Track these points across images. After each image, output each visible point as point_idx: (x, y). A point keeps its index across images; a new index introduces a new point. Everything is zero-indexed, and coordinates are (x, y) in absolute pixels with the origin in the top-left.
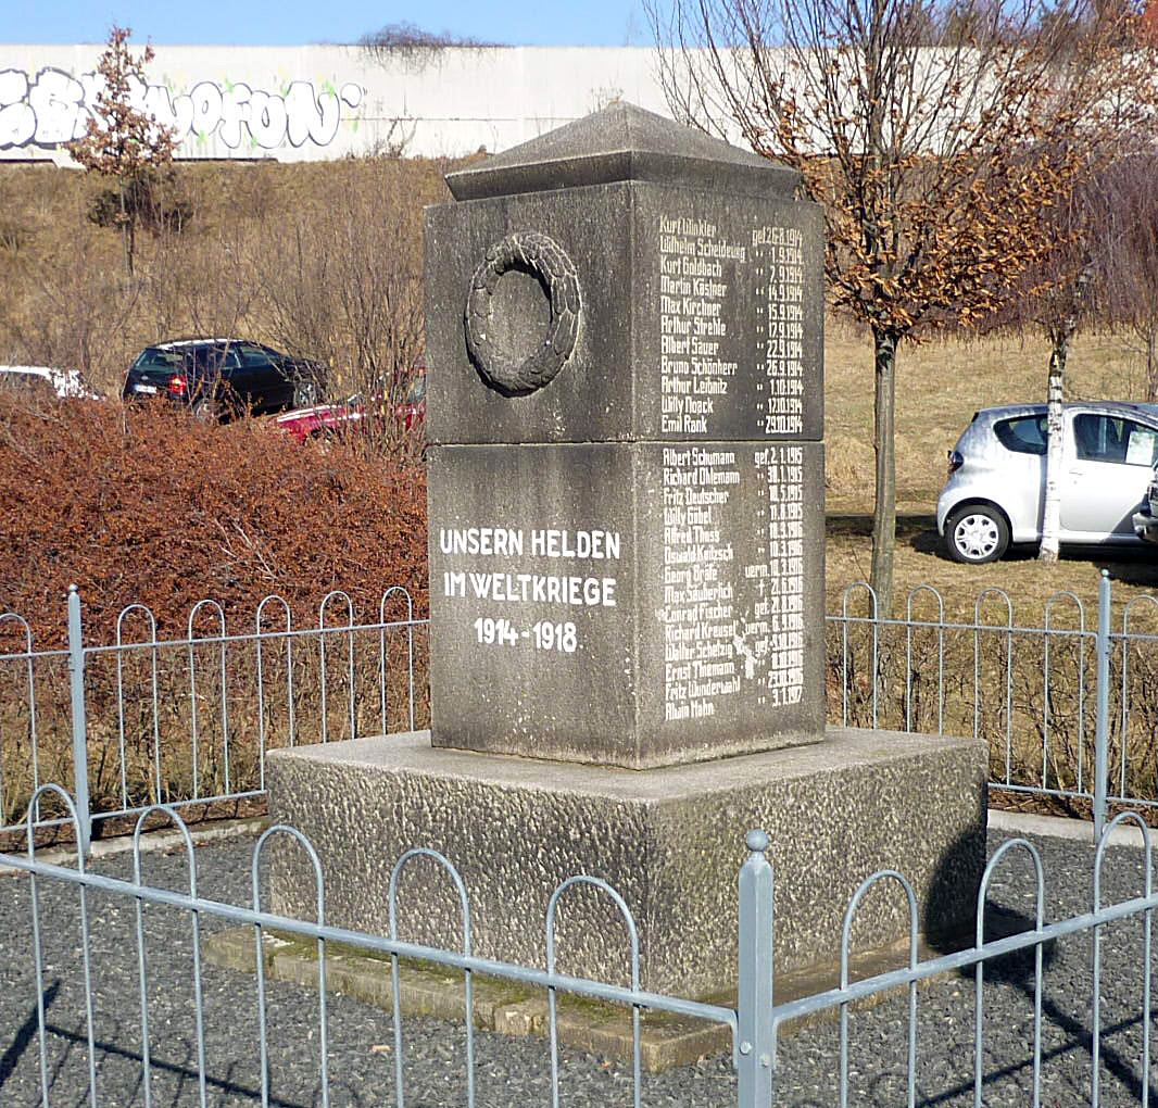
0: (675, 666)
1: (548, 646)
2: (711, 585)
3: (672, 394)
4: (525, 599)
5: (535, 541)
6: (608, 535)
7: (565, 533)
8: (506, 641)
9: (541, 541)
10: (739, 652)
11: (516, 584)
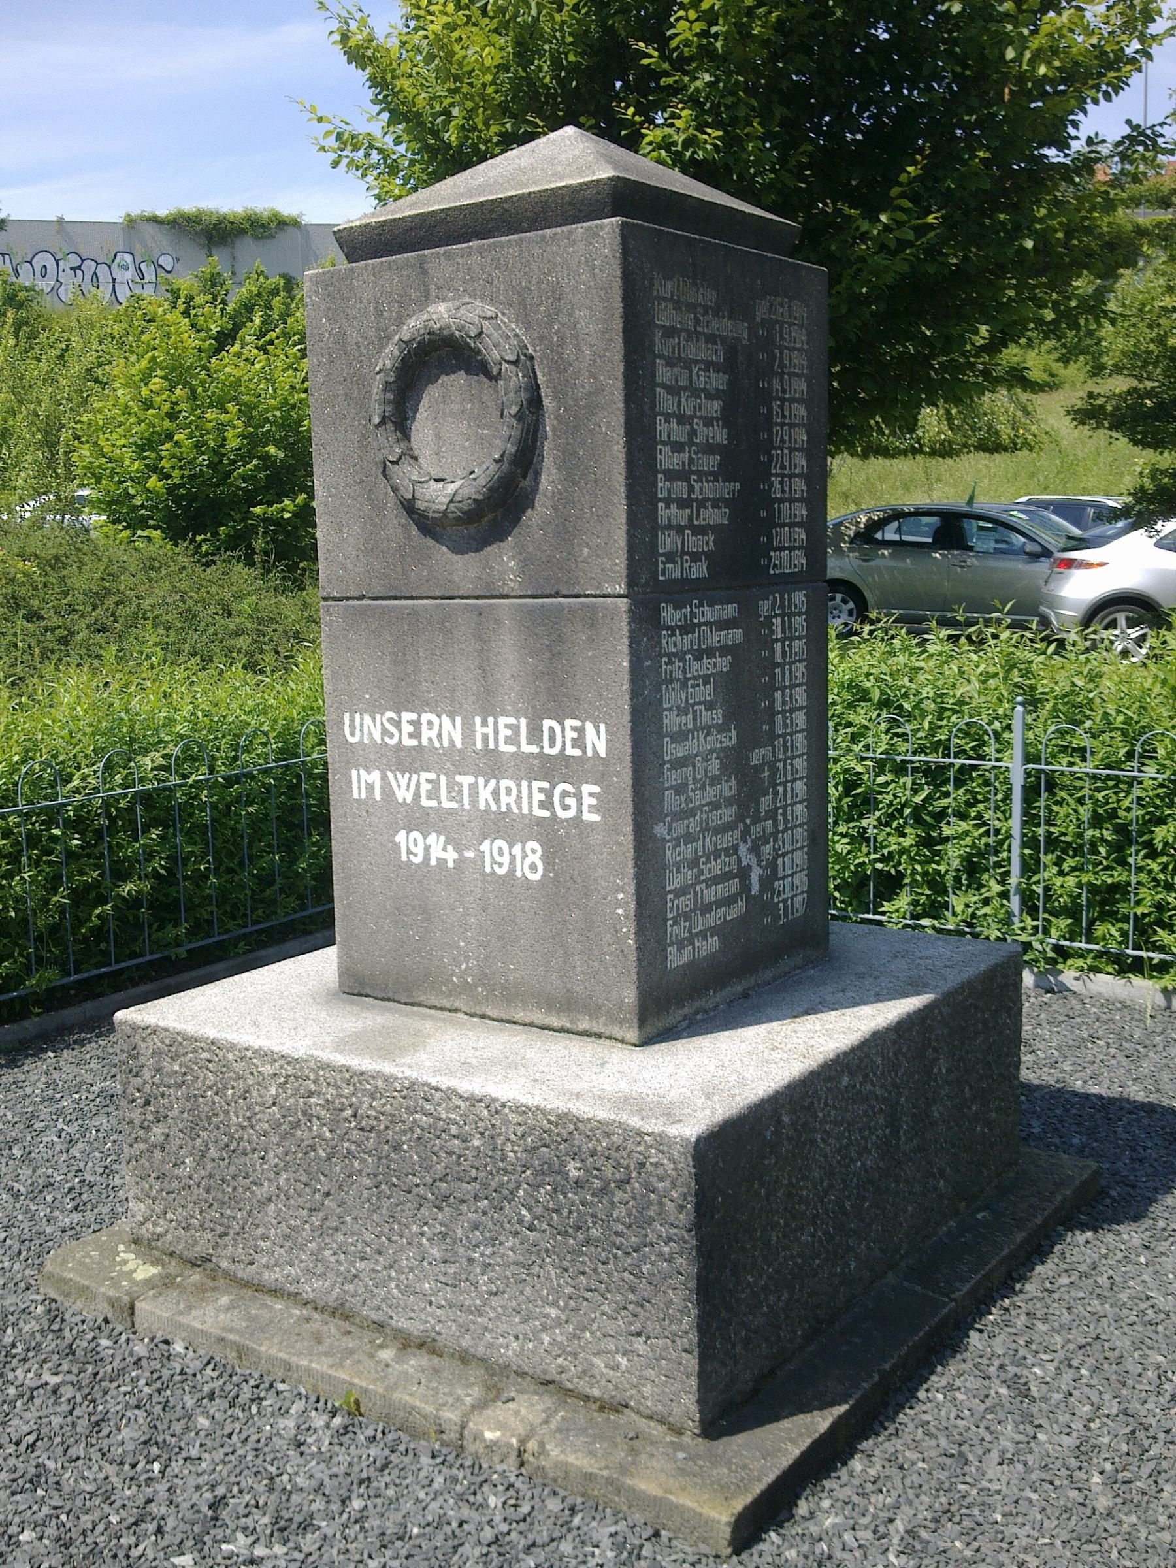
0: (677, 896)
1: (501, 871)
2: (714, 781)
3: (669, 527)
4: (467, 806)
5: (479, 731)
6: (589, 726)
7: (523, 721)
8: (442, 862)
9: (490, 730)
10: (745, 863)
11: (453, 786)
